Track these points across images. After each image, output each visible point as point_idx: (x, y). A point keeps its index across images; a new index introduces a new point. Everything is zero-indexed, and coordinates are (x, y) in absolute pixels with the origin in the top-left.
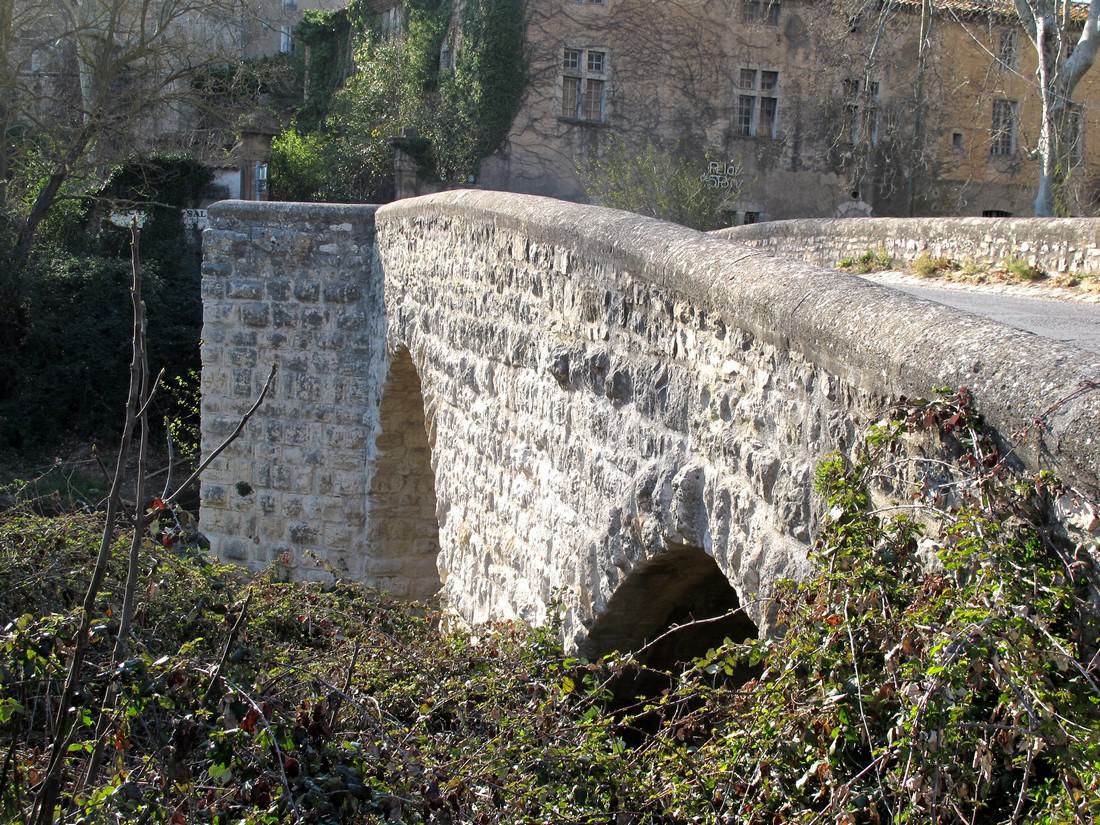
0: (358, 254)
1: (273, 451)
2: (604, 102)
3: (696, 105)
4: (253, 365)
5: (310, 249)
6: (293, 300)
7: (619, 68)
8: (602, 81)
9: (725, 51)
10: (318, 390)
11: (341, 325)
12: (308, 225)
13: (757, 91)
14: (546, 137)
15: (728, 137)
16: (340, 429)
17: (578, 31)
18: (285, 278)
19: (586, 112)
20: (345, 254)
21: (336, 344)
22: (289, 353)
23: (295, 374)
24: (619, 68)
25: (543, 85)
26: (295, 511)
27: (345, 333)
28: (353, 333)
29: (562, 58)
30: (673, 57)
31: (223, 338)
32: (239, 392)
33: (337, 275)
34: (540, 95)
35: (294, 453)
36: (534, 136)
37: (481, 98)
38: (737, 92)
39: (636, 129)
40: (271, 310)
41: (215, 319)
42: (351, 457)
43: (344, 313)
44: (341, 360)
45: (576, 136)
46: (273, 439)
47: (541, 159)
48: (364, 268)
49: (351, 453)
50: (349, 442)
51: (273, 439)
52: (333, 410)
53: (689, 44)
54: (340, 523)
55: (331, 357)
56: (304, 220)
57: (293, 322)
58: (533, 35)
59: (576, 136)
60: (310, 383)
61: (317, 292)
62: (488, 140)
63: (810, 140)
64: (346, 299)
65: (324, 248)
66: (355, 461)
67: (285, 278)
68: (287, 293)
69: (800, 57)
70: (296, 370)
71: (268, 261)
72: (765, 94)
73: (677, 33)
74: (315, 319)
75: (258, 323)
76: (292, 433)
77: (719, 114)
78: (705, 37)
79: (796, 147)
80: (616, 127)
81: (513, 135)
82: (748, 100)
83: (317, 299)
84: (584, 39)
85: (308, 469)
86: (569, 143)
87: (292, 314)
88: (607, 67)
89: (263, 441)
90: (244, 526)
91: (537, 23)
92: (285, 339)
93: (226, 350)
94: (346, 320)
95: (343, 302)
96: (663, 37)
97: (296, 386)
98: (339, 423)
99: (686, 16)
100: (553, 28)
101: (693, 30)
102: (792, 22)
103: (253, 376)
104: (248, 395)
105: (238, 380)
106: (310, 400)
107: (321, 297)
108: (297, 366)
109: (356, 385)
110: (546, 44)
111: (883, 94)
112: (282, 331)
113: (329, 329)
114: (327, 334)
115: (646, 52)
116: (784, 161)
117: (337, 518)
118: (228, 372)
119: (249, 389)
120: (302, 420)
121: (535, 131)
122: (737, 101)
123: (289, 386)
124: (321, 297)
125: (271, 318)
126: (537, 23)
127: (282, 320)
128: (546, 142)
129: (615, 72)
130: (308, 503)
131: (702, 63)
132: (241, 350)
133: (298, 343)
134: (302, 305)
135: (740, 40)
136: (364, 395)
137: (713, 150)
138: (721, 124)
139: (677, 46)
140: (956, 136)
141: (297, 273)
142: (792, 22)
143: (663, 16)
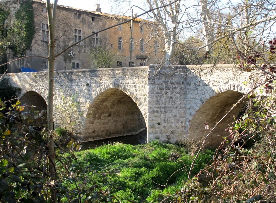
1: (166, 115)
3: (67, 38)
4: (161, 98)
5: (173, 74)
6: (170, 84)
9: (72, 25)
11: (180, 89)
13: (78, 35)
14: (39, 45)
16: (180, 109)
17: (44, 19)
18: (168, 80)
19: (46, 39)
21: (180, 93)
22: (169, 95)
23: (170, 99)
25: (38, 32)
26: (171, 127)
30: (62, 26)
31: (154, 93)
32: (157, 104)
34: (37, 35)
35: (170, 115)
37: (26, 35)
38: (74, 35)
44: (180, 96)
45: (45, 45)
46: (166, 113)
49: (183, 114)
50: (182, 112)
51: (166, 113)
52: (179, 106)
53: (65, 23)
55: (178, 95)
58: (35, 20)
63: (87, 46)
65: (176, 74)
66: (184, 115)
67: (168, 80)
68: (169, 83)
69: (85, 27)
71: (164, 77)
72: (79, 35)
73: (63, 21)
74: (175, 88)
75: (161, 89)
76: (170, 111)
77: (71, 40)
78: (68, 22)
79: (85, 47)
81: (32, 45)
82: (76, 36)
84: (45, 21)
85: (173, 118)
87: (170, 87)
90: (159, 132)
91: (36, 17)
92: (168, 92)
93: (154, 95)
94: (182, 88)
96: (60, 21)
97: (171, 102)
99: (64, 16)
100: (39, 18)
101: (66, 20)
102: (83, 18)
103: (161, 100)
106: (174, 104)
108: (171, 98)
109: (184, 100)
110: (38, 22)
112: (168, 91)
113: (178, 90)
115: (57, 25)
116: (83, 51)
118: (155, 100)
120: (172, 108)
122: (74, 37)
123: (169, 102)
124: (176, 84)
125: (165, 88)
126: (36, 17)
127: (167, 88)
128: (39, 46)
130: (173, 125)
131: (67, 28)
133: (171, 93)
134: (172, 85)
135: (74, 23)
139: (63, 24)
140: (112, 45)
141: (170, 79)
142: (83, 18)
143: (60, 16)
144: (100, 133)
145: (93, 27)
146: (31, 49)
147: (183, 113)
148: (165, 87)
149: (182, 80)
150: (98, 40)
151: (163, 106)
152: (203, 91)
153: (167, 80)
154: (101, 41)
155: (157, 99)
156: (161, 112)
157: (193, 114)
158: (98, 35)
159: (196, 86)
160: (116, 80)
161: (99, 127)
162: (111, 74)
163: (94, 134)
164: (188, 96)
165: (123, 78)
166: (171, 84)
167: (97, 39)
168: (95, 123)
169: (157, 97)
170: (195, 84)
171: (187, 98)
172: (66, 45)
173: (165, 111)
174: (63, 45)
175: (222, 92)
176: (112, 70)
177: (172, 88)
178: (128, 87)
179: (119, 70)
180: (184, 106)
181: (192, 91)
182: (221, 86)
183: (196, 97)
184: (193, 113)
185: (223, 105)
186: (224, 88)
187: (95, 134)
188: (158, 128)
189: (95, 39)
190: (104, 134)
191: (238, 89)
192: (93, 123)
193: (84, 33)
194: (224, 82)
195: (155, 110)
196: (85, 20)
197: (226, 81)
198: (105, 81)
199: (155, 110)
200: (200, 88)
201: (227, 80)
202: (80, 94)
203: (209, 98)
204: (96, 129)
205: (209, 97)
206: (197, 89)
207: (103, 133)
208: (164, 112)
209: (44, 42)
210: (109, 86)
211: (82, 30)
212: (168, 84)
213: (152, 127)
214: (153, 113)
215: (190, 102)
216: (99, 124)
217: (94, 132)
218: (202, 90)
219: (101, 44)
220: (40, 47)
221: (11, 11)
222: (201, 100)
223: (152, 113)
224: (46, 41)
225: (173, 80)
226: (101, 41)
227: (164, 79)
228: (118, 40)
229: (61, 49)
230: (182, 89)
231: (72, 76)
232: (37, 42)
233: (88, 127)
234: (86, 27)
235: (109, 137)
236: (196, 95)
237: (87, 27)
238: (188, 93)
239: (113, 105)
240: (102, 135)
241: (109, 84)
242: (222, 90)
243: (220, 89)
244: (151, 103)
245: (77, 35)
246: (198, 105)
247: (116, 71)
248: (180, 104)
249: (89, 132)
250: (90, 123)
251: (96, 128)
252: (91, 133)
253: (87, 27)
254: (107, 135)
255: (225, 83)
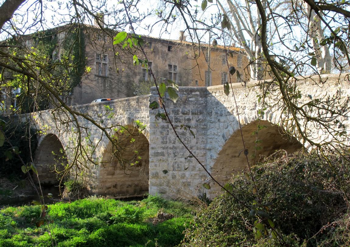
0: (202, 101)
1: (175, 159)
2: (107, 70)
3: (131, 72)
4: (168, 134)
5: (186, 100)
6: (181, 115)
7: (111, 60)
8: (106, 64)
10: (190, 140)
11: (197, 121)
12: (185, 93)
15: (140, 81)
19: (102, 73)
20: (197, 101)
24: (111, 60)
27: (198, 123)
28: (201, 123)
29: (95, 56)
30: (125, 57)
32: (163, 143)
33: (195, 107)
36: (88, 80)
38: (142, 68)
39: (116, 78)
40: (173, 118)
41: (154, 121)
42: (201, 159)
43: (198, 117)
44: (198, 131)
45: (100, 81)
46: (175, 156)
47: (91, 88)
48: (204, 104)
49: (201, 158)
52: (195, 146)
54: (198, 179)
56: (184, 91)
57: (181, 121)
58: (87, 49)
59: (100, 81)
60: (188, 138)
61: (189, 112)
62: (76, 81)
64: (199, 114)
65: (190, 99)
66: (203, 160)
67: (178, 108)
68: (179, 113)
69: (157, 58)
70: (183, 135)
76: (182, 154)
80: (110, 78)
82: (144, 70)
83: (189, 114)
86: (98, 83)
87: (181, 118)
88: (107, 60)
89: (172, 157)
93: (158, 130)
94: (199, 120)
95: (198, 114)
98: (197, 150)
103: (168, 138)
104: (166, 143)
105: (163, 139)
107: (190, 113)
109: (203, 138)
111: (178, 69)
114: (193, 124)
117: (197, 177)
118: (159, 137)
119: (167, 142)
121: (89, 79)
122: (142, 71)
124: (190, 113)
125: (174, 120)
126: (88, 46)
128: (92, 82)
129: (110, 61)
132: (164, 130)
136: (206, 141)
137: (136, 85)
138: (138, 77)
141: (182, 107)
144: (125, 189)
145: (169, 59)
146: (81, 85)
147: (202, 156)
148: (173, 118)
149: (200, 108)
150: (177, 75)
151: (171, 145)
152: (226, 123)
153: (176, 109)
154: (181, 77)
155: (162, 135)
156: (169, 154)
157: (215, 158)
158: (176, 69)
159: (217, 116)
160: (130, 113)
161: (123, 180)
162: (126, 106)
163: (115, 189)
164: (209, 131)
165: (138, 110)
166: (184, 114)
167: (175, 74)
168: (116, 174)
169: (161, 133)
170: (217, 113)
171: (208, 135)
172: (130, 81)
173: (174, 153)
174: (127, 81)
175: (248, 124)
176: (127, 100)
177: (185, 120)
178: (143, 122)
179: (133, 100)
180: (202, 146)
181: (213, 124)
182: (247, 114)
183: (218, 133)
184: (215, 156)
185: (269, 147)
186: (250, 117)
187: (117, 190)
188: (164, 177)
189: (173, 74)
190: (131, 190)
191: (267, 117)
192: (113, 174)
193: (156, 66)
194: (251, 108)
195: (158, 151)
196: (158, 50)
197: (252, 106)
198: (119, 116)
199: (159, 151)
200: (222, 119)
201: (254, 104)
202: (95, 136)
203: (234, 133)
204: (118, 183)
205: (233, 131)
206: (219, 120)
207: (129, 189)
208: (173, 155)
209: (99, 76)
210: (124, 122)
211: (154, 61)
212: (178, 114)
213: (154, 175)
214: (157, 156)
215: (211, 140)
216: (122, 176)
217: (115, 186)
218: (224, 122)
219: (181, 80)
220: (94, 84)
221: (59, 40)
222: (223, 137)
223: (155, 156)
224: (102, 75)
225: (186, 108)
226: (181, 77)
227: (172, 107)
228: (206, 75)
229: (123, 86)
230: (200, 122)
231: (87, 111)
232: (89, 77)
233: (104, 180)
234: (159, 58)
235: (140, 194)
236: (218, 129)
237: (160, 58)
238: (208, 126)
239: (142, 151)
240: (127, 192)
241: (123, 120)
242: (248, 119)
243: (245, 118)
244: (153, 142)
245: (146, 68)
246: (219, 144)
247: (131, 101)
248: (197, 143)
249: (106, 187)
250: (108, 174)
251: (118, 181)
252: (110, 188)
253: (160, 58)
254: (135, 192)
255: (251, 110)
